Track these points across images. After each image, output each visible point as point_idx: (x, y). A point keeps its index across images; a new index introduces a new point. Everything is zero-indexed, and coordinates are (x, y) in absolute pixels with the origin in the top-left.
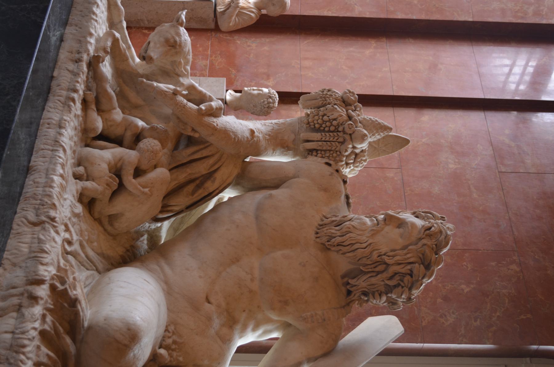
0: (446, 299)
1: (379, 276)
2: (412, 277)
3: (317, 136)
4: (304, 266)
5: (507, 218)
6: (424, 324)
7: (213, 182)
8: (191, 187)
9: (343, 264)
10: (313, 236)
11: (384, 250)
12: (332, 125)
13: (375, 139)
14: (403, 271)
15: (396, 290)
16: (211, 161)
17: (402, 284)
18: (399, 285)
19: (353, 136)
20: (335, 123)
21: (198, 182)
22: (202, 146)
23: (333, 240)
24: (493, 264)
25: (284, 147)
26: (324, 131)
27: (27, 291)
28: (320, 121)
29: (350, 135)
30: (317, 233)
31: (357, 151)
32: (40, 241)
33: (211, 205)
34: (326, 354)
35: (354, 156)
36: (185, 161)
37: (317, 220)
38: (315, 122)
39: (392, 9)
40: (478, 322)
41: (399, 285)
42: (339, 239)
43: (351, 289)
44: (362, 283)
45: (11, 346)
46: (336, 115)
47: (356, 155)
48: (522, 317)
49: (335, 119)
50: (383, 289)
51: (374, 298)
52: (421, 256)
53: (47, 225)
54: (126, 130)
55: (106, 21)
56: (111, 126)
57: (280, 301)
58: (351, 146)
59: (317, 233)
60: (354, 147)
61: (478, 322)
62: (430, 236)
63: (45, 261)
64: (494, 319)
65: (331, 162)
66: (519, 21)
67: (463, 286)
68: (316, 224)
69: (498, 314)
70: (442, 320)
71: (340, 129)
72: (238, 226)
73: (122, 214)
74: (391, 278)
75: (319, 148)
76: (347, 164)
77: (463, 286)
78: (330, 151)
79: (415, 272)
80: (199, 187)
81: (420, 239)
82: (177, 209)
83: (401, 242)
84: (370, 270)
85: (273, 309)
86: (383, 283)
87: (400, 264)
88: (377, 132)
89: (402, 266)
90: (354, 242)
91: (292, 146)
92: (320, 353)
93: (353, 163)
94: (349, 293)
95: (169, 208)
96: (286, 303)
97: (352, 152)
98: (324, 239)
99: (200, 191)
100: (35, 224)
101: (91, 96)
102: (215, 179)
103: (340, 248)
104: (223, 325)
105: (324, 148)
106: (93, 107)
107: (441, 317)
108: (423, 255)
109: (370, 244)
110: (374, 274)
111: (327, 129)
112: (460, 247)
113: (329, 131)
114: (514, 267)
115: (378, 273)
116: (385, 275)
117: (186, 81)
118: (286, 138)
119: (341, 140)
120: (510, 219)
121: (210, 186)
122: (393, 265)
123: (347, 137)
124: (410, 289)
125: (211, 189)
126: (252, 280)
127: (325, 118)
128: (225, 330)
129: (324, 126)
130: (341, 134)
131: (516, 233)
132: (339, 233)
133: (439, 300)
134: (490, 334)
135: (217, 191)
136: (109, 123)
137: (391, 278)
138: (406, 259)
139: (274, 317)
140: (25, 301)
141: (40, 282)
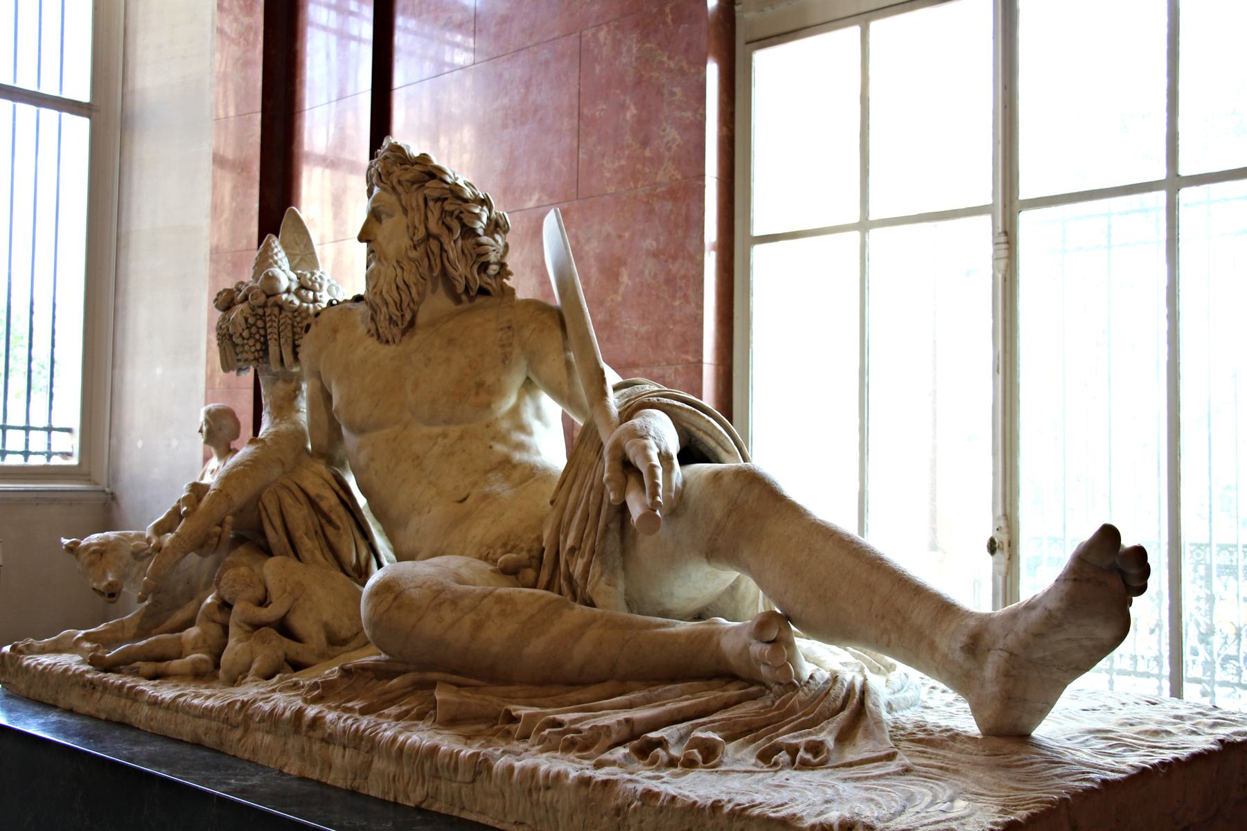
0: (645, 143)
1: (446, 247)
2: (446, 199)
3: (273, 348)
4: (430, 360)
5: (535, 49)
6: (679, 177)
7: (322, 498)
8: (330, 531)
9: (439, 302)
10: (392, 347)
11: (406, 242)
12: (255, 324)
13: (286, 260)
14: (437, 213)
15: (465, 221)
16: (288, 501)
17: (457, 212)
18: (459, 219)
19: (269, 293)
20: (251, 320)
21: (323, 521)
22: (264, 515)
23: (394, 318)
24: (598, 68)
25: (296, 397)
26: (265, 336)
27: (307, 731)
28: (251, 342)
29: (268, 297)
30: (387, 342)
31: (294, 287)
32: (262, 720)
33: (362, 501)
34: (563, 326)
35: (303, 292)
36: (286, 540)
37: (371, 343)
38: (253, 349)
39: (244, 242)
40: (677, 90)
41: (459, 219)
42: (393, 309)
43: (476, 288)
44: (461, 271)
45: (355, 748)
46: (241, 320)
47: (302, 287)
48: (669, 19)
49: (246, 320)
50: (471, 241)
51: (487, 253)
52: (416, 186)
53: (250, 711)
54: (214, 621)
55: (822, 819)
56: (205, 641)
57: (477, 394)
58: (284, 296)
59: (387, 342)
60: (288, 291)
61: (677, 90)
62: (389, 174)
63: (280, 711)
64: (672, 65)
65: (305, 323)
66: (261, 38)
67: (628, 115)
68: (377, 343)
69: (665, 59)
70: (674, 147)
71: (260, 311)
72: (372, 459)
73: (326, 626)
74: (450, 230)
75: (290, 341)
76: (315, 301)
77: (628, 115)
78: (293, 326)
79: (436, 194)
80: (330, 522)
81: (394, 188)
82: (364, 553)
83: (399, 216)
84: (438, 261)
85: (488, 406)
86: (460, 242)
87: (426, 218)
88: (272, 257)
89: (429, 214)
90: (394, 287)
91: (294, 384)
92: (558, 333)
93: (315, 291)
94: (483, 291)
95: (363, 563)
96: (480, 385)
97: (297, 293)
98: (396, 331)
99: (334, 517)
100: (246, 730)
101: (148, 667)
102: (318, 496)
103: (405, 305)
104: (507, 478)
105: (290, 335)
106: (163, 665)
107: (669, 149)
108: (413, 183)
109: (398, 262)
110: (444, 255)
111: (262, 332)
112: (576, 122)
113: (265, 328)
114: (602, 35)
115: (442, 249)
116: (445, 240)
117: (148, 534)
118: (281, 394)
119: (276, 311)
120: (536, 44)
121: (330, 501)
122: (427, 228)
123: (271, 300)
124: (466, 201)
125: (334, 500)
126: (445, 436)
127: (246, 334)
128: (516, 475)
129: (257, 337)
130: (268, 311)
131: (556, 34)
132: (384, 309)
133: (648, 153)
134: (693, 71)
135: (341, 493)
136: (200, 644)
137: (450, 230)
138: (419, 209)
139: (511, 401)
140: (318, 734)
141: (299, 713)
